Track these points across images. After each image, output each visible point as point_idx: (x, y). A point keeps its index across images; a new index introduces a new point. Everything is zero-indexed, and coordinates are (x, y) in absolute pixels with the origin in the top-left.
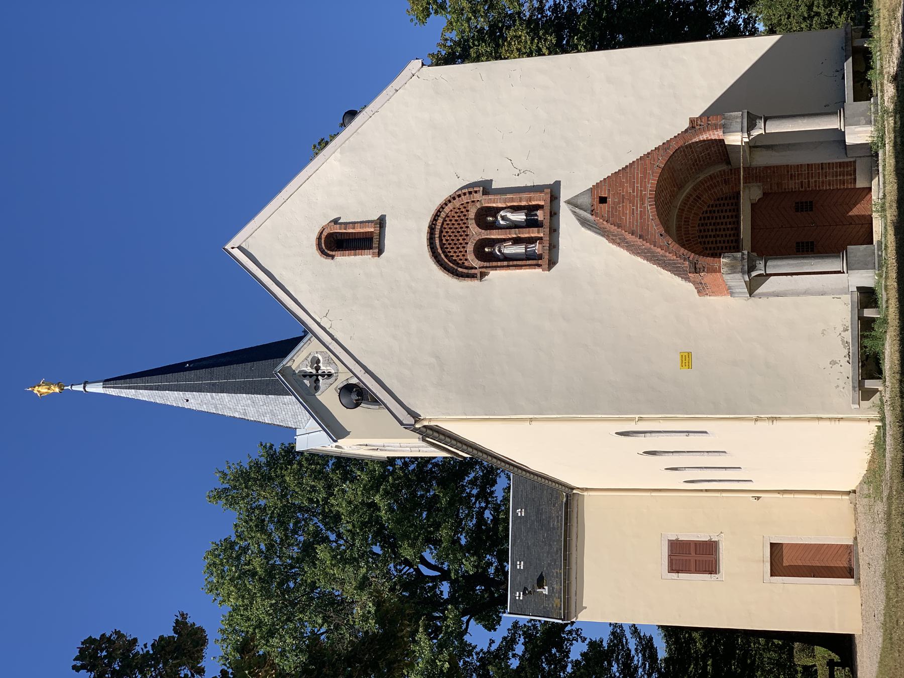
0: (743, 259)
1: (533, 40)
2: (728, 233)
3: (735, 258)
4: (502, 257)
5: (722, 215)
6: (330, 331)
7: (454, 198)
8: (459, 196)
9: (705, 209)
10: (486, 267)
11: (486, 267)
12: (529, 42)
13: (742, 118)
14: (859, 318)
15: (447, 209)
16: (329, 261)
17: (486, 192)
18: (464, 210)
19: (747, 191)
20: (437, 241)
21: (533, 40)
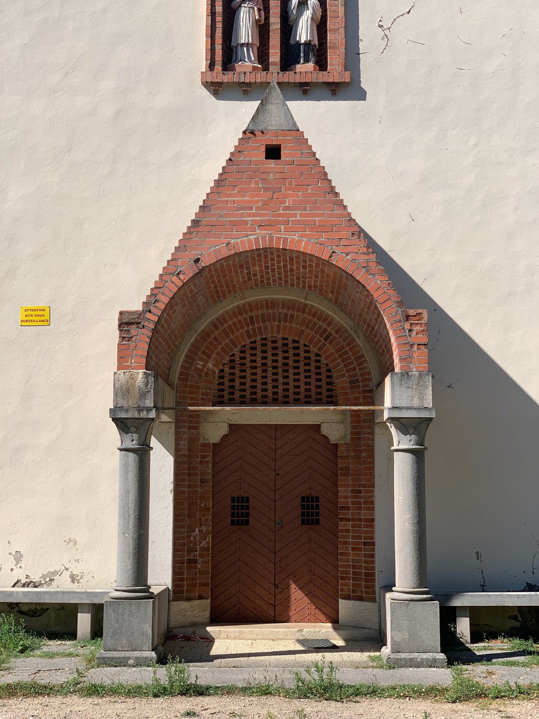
0: (140, 409)
2: (269, 386)
3: (143, 395)
13: (418, 409)
19: (338, 418)
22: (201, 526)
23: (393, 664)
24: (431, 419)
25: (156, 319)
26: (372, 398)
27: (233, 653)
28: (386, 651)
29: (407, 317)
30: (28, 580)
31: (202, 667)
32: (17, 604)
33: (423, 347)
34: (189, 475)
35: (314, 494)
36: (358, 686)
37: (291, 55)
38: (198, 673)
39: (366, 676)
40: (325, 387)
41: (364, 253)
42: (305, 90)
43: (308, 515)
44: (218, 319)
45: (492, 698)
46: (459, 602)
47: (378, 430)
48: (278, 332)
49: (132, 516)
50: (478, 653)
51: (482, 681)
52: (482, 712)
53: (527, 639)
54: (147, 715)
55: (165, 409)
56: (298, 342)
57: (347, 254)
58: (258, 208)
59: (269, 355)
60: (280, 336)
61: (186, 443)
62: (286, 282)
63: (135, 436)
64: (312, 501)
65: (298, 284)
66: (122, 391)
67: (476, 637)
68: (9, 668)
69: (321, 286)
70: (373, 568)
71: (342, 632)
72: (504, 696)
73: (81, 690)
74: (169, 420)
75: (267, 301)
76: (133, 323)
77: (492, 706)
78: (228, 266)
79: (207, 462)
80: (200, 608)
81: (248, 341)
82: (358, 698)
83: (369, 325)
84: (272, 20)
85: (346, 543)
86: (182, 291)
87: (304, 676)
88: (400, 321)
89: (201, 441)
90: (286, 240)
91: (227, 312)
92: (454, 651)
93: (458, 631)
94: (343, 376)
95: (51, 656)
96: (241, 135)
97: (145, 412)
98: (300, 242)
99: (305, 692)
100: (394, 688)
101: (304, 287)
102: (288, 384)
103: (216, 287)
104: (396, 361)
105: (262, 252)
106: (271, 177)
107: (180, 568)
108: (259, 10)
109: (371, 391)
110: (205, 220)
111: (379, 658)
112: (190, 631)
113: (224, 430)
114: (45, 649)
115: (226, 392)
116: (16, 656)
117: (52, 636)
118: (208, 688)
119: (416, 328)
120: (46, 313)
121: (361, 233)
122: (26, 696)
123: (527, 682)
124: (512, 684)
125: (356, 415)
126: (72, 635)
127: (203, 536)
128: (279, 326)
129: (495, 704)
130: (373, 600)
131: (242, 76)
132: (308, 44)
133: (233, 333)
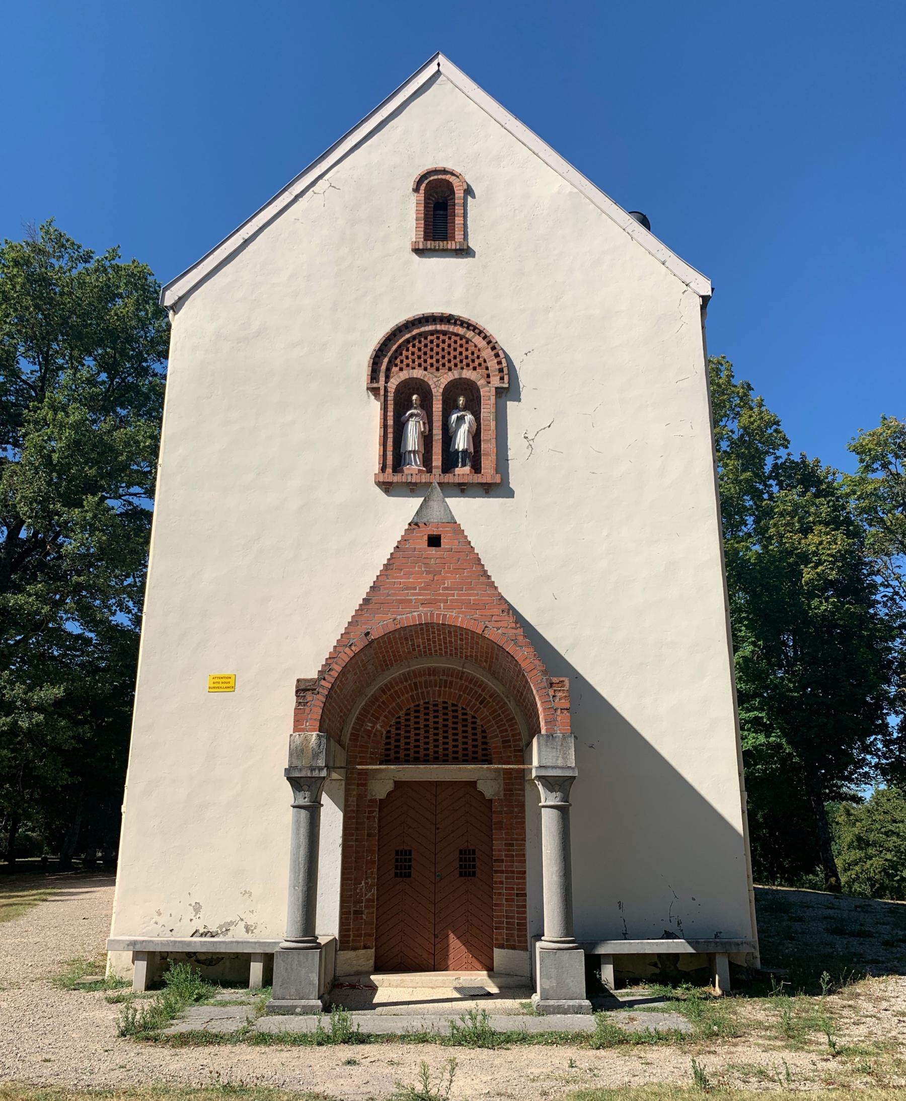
0: (312, 769)
1: (832, 556)
2: (431, 746)
3: (316, 756)
4: (403, 419)
5: (460, 737)
6: (310, 193)
7: (493, 348)
8: (497, 355)
9: (468, 711)
10: (386, 396)
11: (386, 396)
12: (829, 552)
14: (249, 955)
15: (478, 341)
16: (411, 185)
17: (500, 392)
18: (476, 363)
19: (493, 775)
20: (430, 328)
21: (832, 556)
22: (366, 879)
23: (542, 1011)
24: (575, 777)
25: (329, 686)
26: (523, 756)
27: (395, 1001)
28: (536, 998)
29: (551, 685)
30: (206, 930)
31: (365, 1015)
32: (195, 953)
33: (565, 712)
34: (357, 829)
35: (471, 848)
36: (509, 1033)
37: (450, 460)
38: (361, 1021)
39: (517, 1023)
40: (480, 747)
41: (512, 628)
42: (463, 489)
43: (465, 868)
44: (386, 685)
45: (634, 1044)
46: (603, 950)
47: (527, 786)
48: (439, 696)
49: (302, 870)
50: (621, 1000)
51: (624, 1027)
52: (624, 1058)
53: (666, 985)
54: (311, 1063)
55: (334, 768)
56: (456, 706)
57: (498, 629)
58: (421, 589)
59: (431, 717)
60: (440, 700)
61: (355, 799)
62: (446, 652)
63: (307, 794)
64: (469, 854)
65: (456, 653)
66: (296, 752)
67: (619, 984)
68: (183, 1017)
69: (476, 656)
70: (525, 918)
71: (496, 979)
72: (645, 1042)
73: (250, 1038)
74: (340, 778)
75: (429, 669)
76: (308, 690)
77: (633, 1053)
78: (395, 638)
79: (374, 817)
80: (364, 958)
81: (412, 705)
82: (508, 1046)
83: (518, 691)
84: (434, 432)
85: (500, 894)
86: (353, 661)
87: (459, 1023)
88: (545, 688)
89: (369, 798)
90: (445, 616)
91: (394, 679)
92: (599, 998)
93: (603, 978)
94: (497, 736)
95: (224, 1004)
96: (407, 527)
97: (317, 771)
98: (457, 618)
99: (461, 1039)
100: (542, 1035)
101: (461, 657)
102: (447, 743)
103: (384, 656)
104: (542, 724)
105: (424, 626)
106: (432, 561)
107: (347, 919)
108: (424, 423)
109: (521, 751)
110: (375, 599)
111: (530, 1005)
112: (354, 979)
113: (390, 786)
114: (219, 997)
115: (392, 751)
116: (191, 1005)
117: (227, 984)
118: (369, 1036)
119: (559, 694)
120: (232, 681)
121: (511, 610)
122: (197, 1045)
123: (666, 1028)
124: (652, 1030)
125: (508, 772)
126: (245, 984)
127: (369, 888)
128: (439, 691)
129: (636, 1050)
130: (525, 949)
131: (409, 477)
132: (465, 452)
133: (399, 697)
